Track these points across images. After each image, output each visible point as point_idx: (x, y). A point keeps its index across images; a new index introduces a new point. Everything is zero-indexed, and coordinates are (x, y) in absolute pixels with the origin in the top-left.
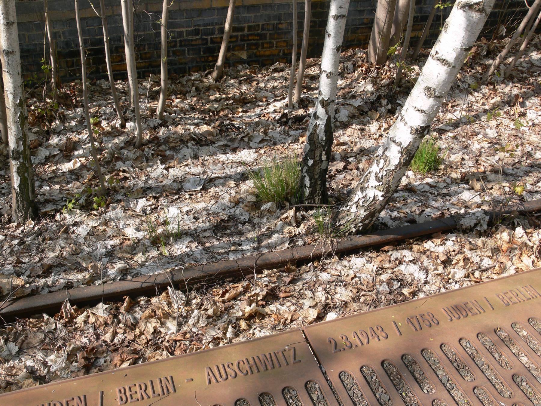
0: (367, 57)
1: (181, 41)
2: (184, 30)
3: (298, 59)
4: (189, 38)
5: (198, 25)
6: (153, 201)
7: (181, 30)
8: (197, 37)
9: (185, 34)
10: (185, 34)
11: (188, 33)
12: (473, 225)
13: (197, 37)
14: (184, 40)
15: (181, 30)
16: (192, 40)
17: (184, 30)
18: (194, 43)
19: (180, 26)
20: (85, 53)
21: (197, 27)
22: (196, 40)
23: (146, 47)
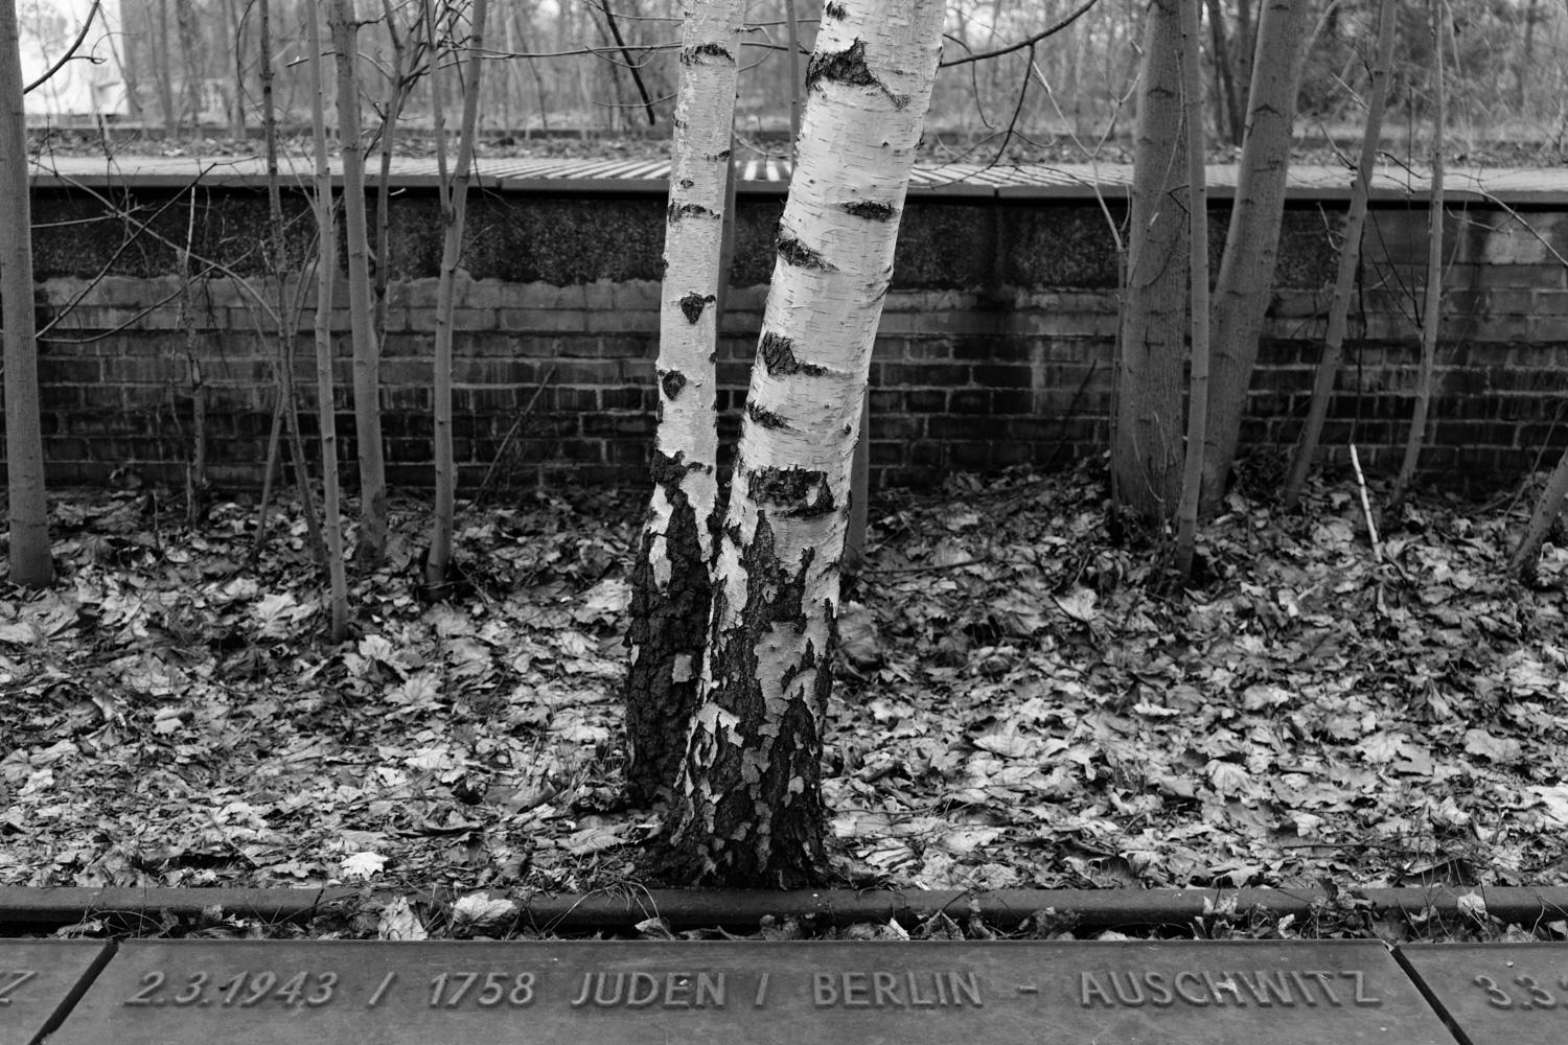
0: (1544, 1007)
1: (587, 420)
2: (598, 388)
3: (1074, 314)
4: (612, 412)
5: (636, 380)
6: (602, 690)
7: (589, 387)
8: (635, 412)
9: (599, 402)
10: (599, 402)
11: (611, 399)
12: (1338, 736)
13: (635, 412)
14: (600, 419)
15: (589, 387)
16: (620, 420)
17: (598, 388)
18: (625, 427)
19: (589, 377)
20: (489, 392)
21: (633, 385)
22: (631, 419)
23: (494, 425)
